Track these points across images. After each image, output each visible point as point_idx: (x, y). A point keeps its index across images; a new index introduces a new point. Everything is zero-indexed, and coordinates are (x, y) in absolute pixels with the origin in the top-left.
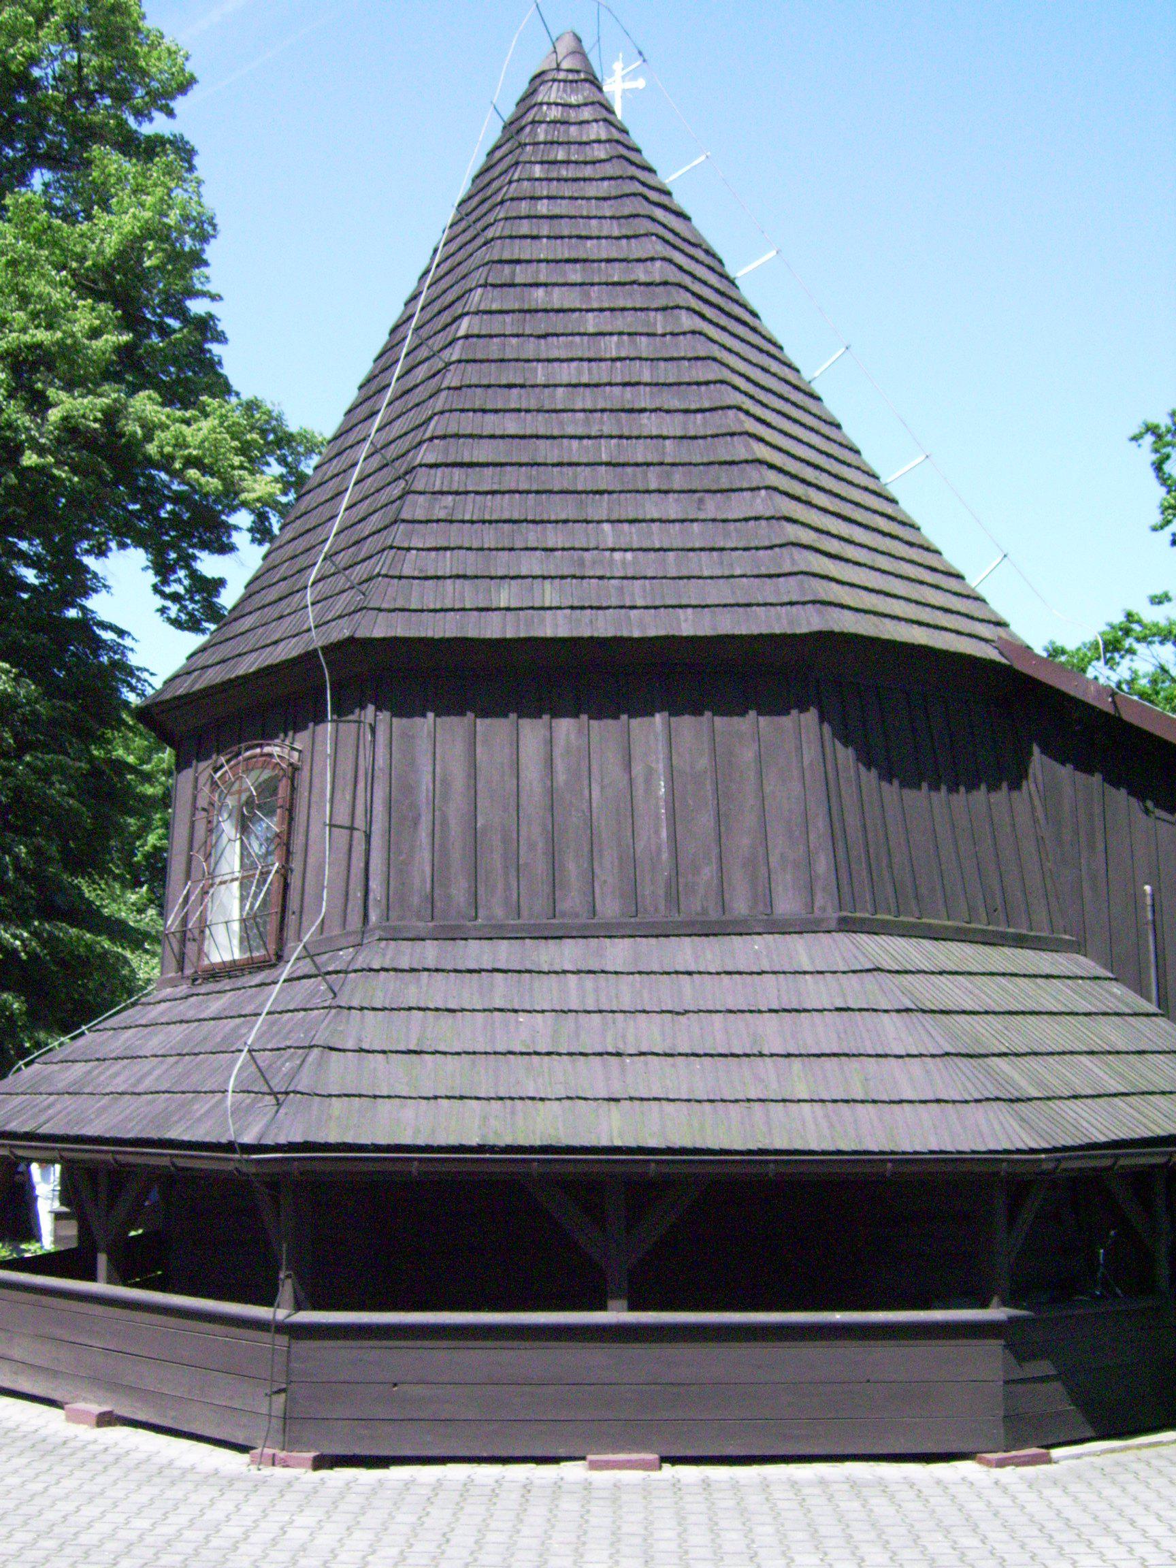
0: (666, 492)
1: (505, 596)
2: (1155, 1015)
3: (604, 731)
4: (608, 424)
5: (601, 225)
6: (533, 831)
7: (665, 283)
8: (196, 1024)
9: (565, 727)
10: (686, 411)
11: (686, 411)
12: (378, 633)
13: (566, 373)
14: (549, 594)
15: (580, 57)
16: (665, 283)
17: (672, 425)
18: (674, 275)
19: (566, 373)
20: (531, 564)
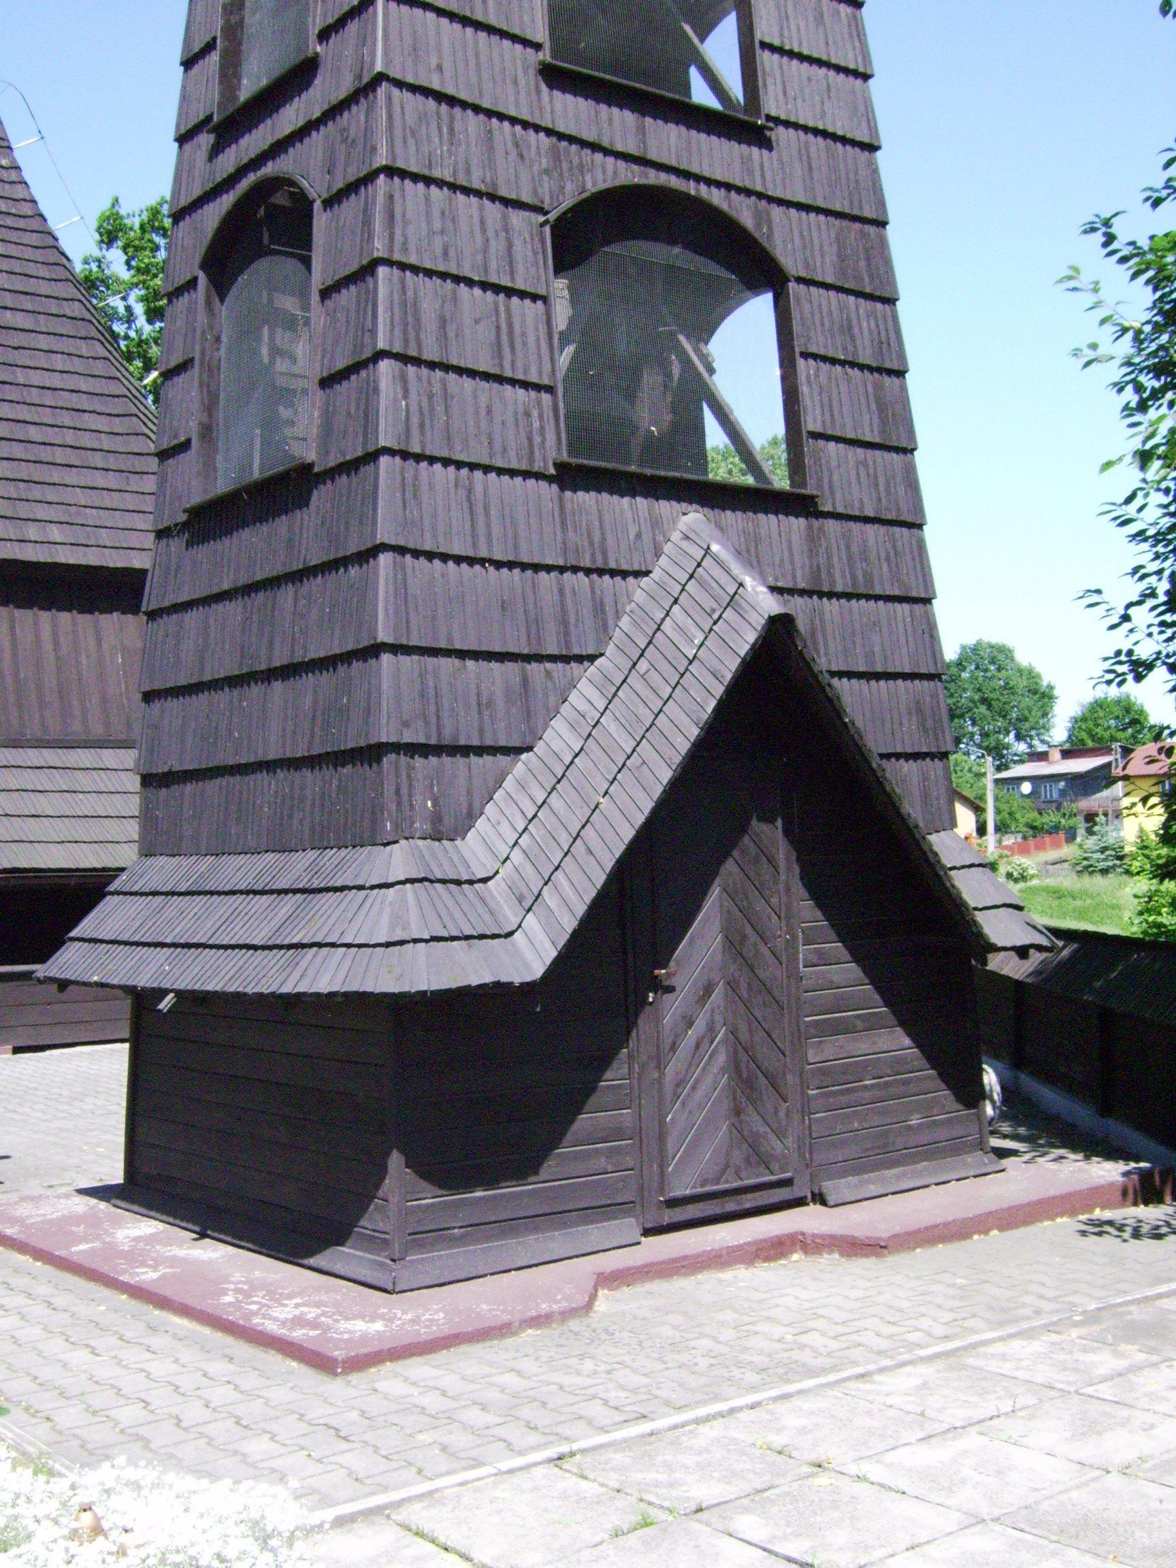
0: (107, 470)
1: (32, 532)
2: (841, 674)
3: (84, 621)
4: (66, 419)
5: (397, 919)
6: (50, 680)
7: (83, 319)
8: (777, 1548)
9: (65, 617)
10: (110, 415)
11: (110, 415)
12: (324, 985)
13: (36, 378)
14: (55, 533)
15: (38, 218)
16: (83, 319)
17: (100, 423)
18: (88, 316)
19: (36, 378)
20: (41, 512)
